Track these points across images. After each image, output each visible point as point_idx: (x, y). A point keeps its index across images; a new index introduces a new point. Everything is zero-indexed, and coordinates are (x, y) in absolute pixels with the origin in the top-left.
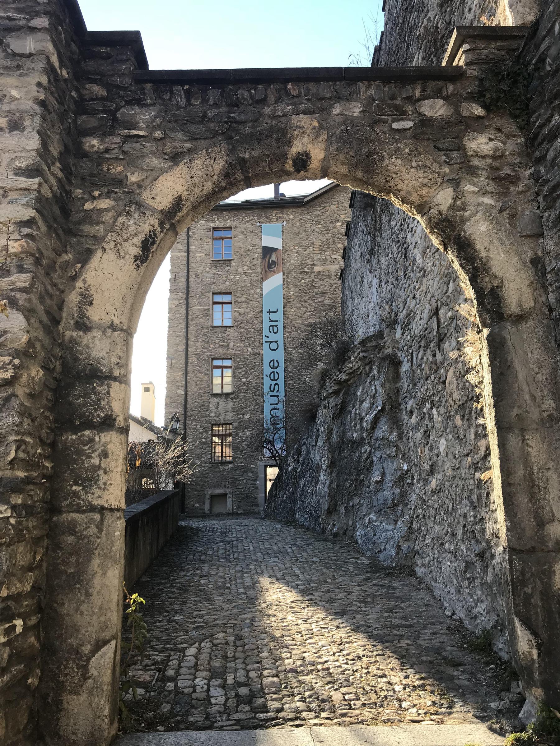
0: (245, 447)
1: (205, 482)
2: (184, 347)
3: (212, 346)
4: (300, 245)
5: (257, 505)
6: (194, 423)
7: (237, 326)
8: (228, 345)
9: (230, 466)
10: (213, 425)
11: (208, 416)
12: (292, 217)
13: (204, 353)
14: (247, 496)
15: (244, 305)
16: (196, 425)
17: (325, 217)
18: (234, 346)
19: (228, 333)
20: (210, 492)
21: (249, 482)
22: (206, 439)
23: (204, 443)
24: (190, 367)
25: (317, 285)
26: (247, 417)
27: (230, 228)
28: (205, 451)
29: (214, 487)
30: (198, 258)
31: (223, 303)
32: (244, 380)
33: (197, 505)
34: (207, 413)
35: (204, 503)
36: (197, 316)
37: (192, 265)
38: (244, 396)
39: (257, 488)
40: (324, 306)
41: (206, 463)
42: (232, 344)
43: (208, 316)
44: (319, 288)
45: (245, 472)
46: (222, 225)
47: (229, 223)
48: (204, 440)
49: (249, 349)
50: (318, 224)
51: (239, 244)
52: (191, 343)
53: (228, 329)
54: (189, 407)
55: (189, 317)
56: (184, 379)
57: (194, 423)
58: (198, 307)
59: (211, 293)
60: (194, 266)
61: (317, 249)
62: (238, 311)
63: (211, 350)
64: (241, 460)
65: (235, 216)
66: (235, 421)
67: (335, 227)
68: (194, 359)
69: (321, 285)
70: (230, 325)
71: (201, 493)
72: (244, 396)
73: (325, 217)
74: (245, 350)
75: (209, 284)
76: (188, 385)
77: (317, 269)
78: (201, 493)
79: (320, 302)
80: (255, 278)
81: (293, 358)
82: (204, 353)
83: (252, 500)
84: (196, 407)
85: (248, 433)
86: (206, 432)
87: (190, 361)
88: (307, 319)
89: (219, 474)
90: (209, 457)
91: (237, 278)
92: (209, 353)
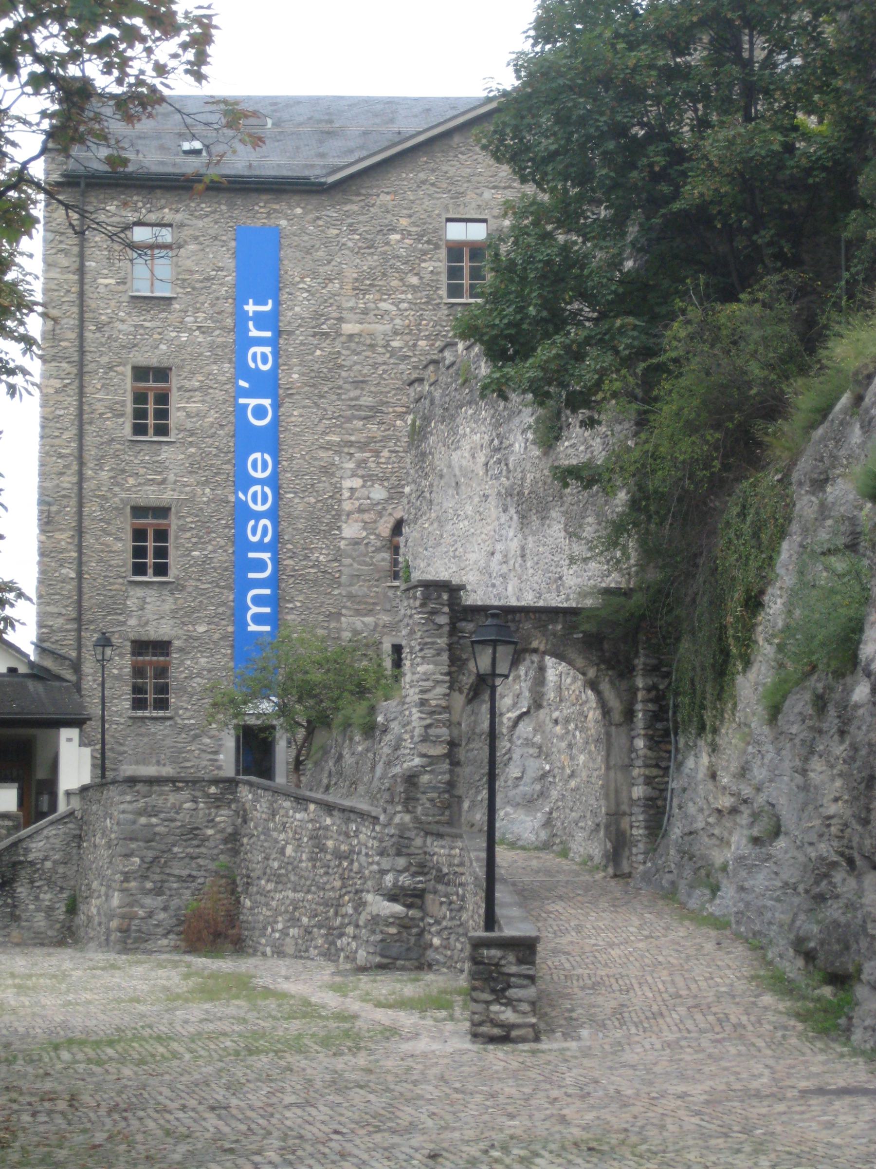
2: (75, 479)
3: (131, 481)
4: (314, 274)
9: (168, 723)
11: (124, 623)
12: (299, 211)
13: (115, 495)
21: (204, 755)
26: (201, 629)
30: (102, 289)
32: (196, 553)
34: (121, 618)
40: (360, 408)
41: (120, 716)
45: (196, 737)
49: (207, 490)
50: (354, 231)
54: (85, 604)
64: (188, 714)
69: (356, 363)
77: (348, 328)
79: (352, 399)
82: (115, 495)
85: (203, 661)
87: (86, 510)
89: (146, 740)
92: (124, 495)
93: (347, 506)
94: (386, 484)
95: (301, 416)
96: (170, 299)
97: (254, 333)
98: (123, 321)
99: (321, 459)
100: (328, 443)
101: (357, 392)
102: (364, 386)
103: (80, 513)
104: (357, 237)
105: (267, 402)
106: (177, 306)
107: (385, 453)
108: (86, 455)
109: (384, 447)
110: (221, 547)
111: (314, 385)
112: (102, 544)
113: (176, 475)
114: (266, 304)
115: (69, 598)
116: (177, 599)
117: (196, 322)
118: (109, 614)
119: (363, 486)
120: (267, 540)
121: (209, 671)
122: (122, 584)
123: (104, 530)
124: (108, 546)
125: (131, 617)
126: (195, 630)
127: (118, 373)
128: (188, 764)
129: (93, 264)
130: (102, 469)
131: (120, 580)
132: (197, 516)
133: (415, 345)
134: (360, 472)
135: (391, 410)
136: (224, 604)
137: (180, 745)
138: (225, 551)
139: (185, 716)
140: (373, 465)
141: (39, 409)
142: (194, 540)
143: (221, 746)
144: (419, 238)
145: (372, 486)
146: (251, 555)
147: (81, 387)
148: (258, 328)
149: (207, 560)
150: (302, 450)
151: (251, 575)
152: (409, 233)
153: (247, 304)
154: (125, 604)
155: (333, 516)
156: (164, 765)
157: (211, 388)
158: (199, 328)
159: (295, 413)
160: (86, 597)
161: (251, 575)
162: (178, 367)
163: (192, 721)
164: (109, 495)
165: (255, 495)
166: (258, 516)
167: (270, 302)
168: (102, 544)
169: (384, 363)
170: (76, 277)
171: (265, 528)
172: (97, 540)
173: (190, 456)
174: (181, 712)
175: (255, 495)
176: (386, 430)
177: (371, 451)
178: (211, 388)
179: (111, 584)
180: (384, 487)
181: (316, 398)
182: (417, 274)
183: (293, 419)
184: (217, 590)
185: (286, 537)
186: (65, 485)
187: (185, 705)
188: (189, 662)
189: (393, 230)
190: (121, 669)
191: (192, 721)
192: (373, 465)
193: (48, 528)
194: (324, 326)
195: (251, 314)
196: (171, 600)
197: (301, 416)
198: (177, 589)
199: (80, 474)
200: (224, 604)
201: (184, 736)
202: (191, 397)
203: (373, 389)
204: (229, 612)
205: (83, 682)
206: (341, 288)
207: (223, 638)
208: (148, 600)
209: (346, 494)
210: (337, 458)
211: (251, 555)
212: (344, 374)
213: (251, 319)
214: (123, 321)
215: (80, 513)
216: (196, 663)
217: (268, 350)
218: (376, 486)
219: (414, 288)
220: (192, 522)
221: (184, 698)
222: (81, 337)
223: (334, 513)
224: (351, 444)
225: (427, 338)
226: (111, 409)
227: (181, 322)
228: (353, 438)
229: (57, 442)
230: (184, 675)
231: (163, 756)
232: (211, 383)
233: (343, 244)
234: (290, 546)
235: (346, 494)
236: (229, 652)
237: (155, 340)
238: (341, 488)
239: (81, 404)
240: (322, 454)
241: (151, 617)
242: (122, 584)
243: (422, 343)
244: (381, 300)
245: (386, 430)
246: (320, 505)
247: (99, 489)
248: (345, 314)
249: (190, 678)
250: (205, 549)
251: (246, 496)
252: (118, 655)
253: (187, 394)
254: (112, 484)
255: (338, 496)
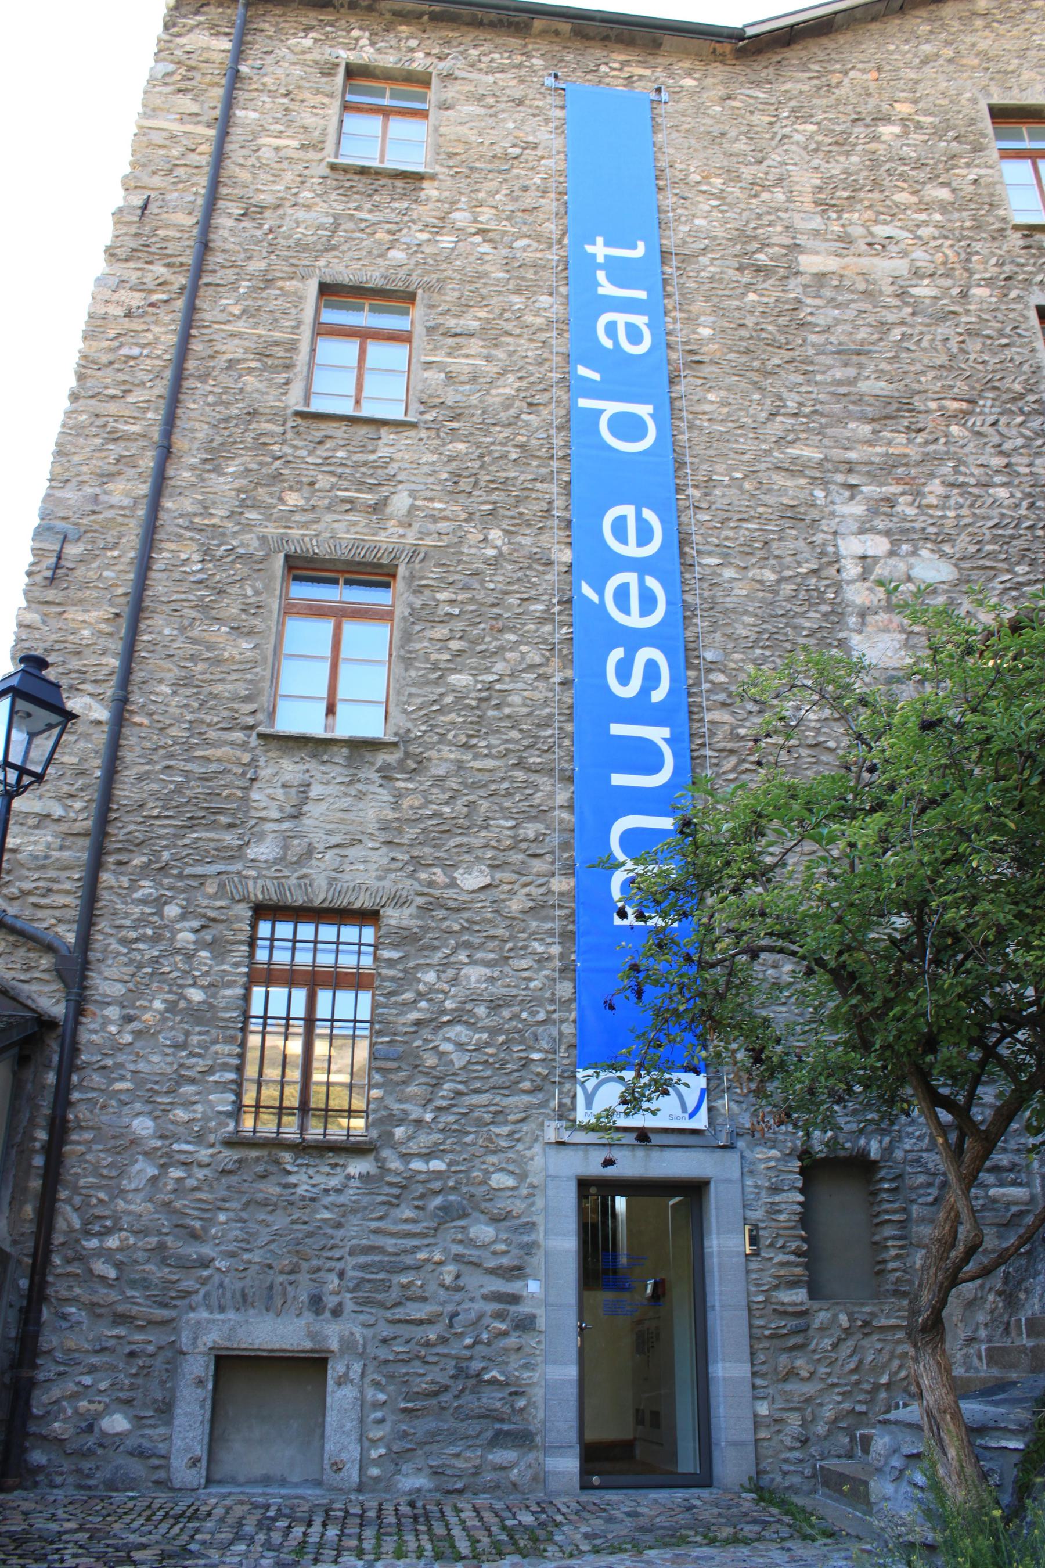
0: (459, 1060)
1: (186, 1266)
2: (144, 489)
3: (293, 499)
4: (732, 176)
5: (523, 1439)
6: (147, 888)
7: (434, 427)
8: (385, 502)
9: (358, 1167)
10: (263, 911)
11: (237, 854)
12: (689, 82)
13: (247, 527)
14: (461, 1372)
15: (475, 346)
16: (159, 903)
17: (832, 100)
18: (413, 508)
19: (383, 452)
20: (212, 1338)
21: (474, 1281)
22: (212, 988)
23: (198, 1015)
24: (159, 585)
25: (821, 320)
26: (471, 880)
27: (423, 80)
28: (201, 1064)
29: (244, 1301)
30: (266, 154)
31: (364, 335)
32: (460, 680)
33: (117, 1423)
34: (230, 838)
35: (165, 1410)
36: (231, 364)
37: (231, 168)
38: (460, 765)
39: (526, 1325)
40: (860, 400)
41: (199, 1138)
42: (401, 502)
43: (288, 367)
44: (828, 329)
45: (448, 1214)
46: (389, 60)
47: (419, 62)
48: (196, 995)
49: (495, 535)
50: (807, 118)
51: (464, 130)
52: (181, 474)
53: (387, 435)
54: (125, 792)
55: (191, 365)
56: (116, 645)
57: (147, 888)
58: (240, 326)
59: (312, 289)
60: (244, 175)
61: (808, 198)
62: (440, 366)
63: (285, 519)
64: (425, 1140)
65: (448, 42)
66: (399, 901)
67: (876, 138)
68: (190, 552)
69: (838, 321)
70: (396, 413)
71: (149, 1340)
72: (460, 765)
73: (832, 100)
74: (474, 535)
75: (306, 248)
76: (138, 676)
77: (810, 263)
78: (149, 1340)
79: (839, 383)
80: (530, 255)
81: (730, 602)
82: (247, 527)
83: (492, 1399)
84: (166, 801)
85: (474, 974)
86: (219, 948)
87: (162, 558)
88: (780, 441)
89: (280, 1221)
90: (223, 1102)
91: (446, 241)
92: (272, 530)
93: (858, 595)
94: (947, 548)
95: (725, 403)
96: (419, 177)
97: (607, 289)
98: (308, 207)
99: (782, 491)
100: (795, 459)
101: (851, 372)
102: (863, 359)
103: (144, 565)
104: (813, 128)
105: (644, 410)
106: (435, 193)
107: (935, 488)
108: (180, 443)
109: (932, 475)
110: (532, 667)
111: (748, 351)
112: (194, 641)
113: (413, 494)
114: (634, 247)
115: (82, 773)
116: (399, 795)
117: (476, 221)
118: (193, 824)
119: (892, 553)
120: (658, 695)
121: (495, 1005)
122: (244, 745)
123: (204, 607)
124: (210, 647)
125: (261, 836)
126: (453, 884)
127: (284, 293)
128: (417, 1311)
129: (253, 115)
130: (218, 470)
131: (238, 736)
132: (466, 588)
133: (964, 295)
134: (881, 524)
135: (933, 405)
136: (541, 814)
137: (389, 1243)
138: (545, 677)
139: (413, 1147)
140: (911, 511)
141: (99, 265)
142: (455, 645)
143: (529, 1249)
144: (939, 133)
145: (914, 553)
146: (617, 729)
147: (192, 309)
148: (612, 280)
149: (489, 695)
150: (731, 469)
151: (619, 779)
152: (919, 126)
153: (594, 256)
154: (245, 799)
155: (825, 615)
156: (337, 1312)
157: (508, 334)
158: (481, 232)
159: (711, 397)
160: (128, 775)
161: (619, 779)
162: (429, 288)
163: (436, 1165)
164: (231, 526)
165: (622, 595)
166: (634, 640)
167: (641, 245)
168: (194, 641)
169: (903, 323)
170: (212, 132)
171: (651, 666)
172: (183, 629)
173: (451, 459)
174: (399, 1132)
175: (622, 595)
176: (927, 443)
177: (899, 481)
178: (508, 334)
179: (207, 743)
180: (943, 555)
181: (755, 377)
182: (943, 184)
183: (707, 407)
184: (520, 775)
185: (709, 655)
186: (115, 499)
187: (415, 1113)
188: (430, 977)
189: (887, 119)
190: (212, 988)
191: (436, 1165)
192: (911, 511)
193: (51, 594)
194: (760, 256)
195: (600, 259)
196: (385, 796)
197: (725, 403)
198: (401, 767)
199: (160, 482)
200: (541, 814)
201: (408, 1213)
202: (460, 347)
203: (883, 366)
204: (555, 839)
205: (89, 1023)
206: (789, 200)
207: (537, 909)
208: (315, 791)
209: (852, 570)
210: (819, 493)
211: (617, 729)
212: (812, 338)
213: (600, 267)
214: (308, 207)
215: (144, 565)
216: (454, 981)
217: (641, 321)
218: (924, 553)
219: (944, 207)
220: (452, 602)
221: (412, 1089)
222: (206, 225)
223: (825, 608)
224: (850, 467)
225: (989, 282)
226: (261, 355)
227: (442, 219)
228: (852, 455)
229: (112, 408)
230: (414, 1016)
231: (333, 1282)
232: (508, 327)
233: (784, 136)
234: (720, 678)
235: (852, 570)
236: (556, 950)
237: (379, 242)
238: (837, 558)
239: (185, 338)
240: (780, 480)
241: (320, 840)
242: (244, 745)
243: (979, 292)
244: (876, 222)
245: (927, 443)
246: (788, 588)
247: (206, 510)
248: (801, 240)
249: (434, 1023)
250: (488, 670)
251: (601, 593)
252: (209, 946)
253: (451, 341)
254: (243, 504)
255: (832, 571)
